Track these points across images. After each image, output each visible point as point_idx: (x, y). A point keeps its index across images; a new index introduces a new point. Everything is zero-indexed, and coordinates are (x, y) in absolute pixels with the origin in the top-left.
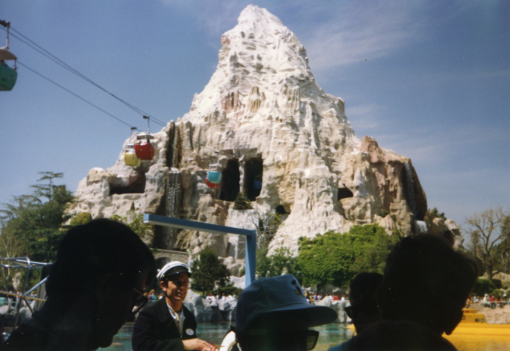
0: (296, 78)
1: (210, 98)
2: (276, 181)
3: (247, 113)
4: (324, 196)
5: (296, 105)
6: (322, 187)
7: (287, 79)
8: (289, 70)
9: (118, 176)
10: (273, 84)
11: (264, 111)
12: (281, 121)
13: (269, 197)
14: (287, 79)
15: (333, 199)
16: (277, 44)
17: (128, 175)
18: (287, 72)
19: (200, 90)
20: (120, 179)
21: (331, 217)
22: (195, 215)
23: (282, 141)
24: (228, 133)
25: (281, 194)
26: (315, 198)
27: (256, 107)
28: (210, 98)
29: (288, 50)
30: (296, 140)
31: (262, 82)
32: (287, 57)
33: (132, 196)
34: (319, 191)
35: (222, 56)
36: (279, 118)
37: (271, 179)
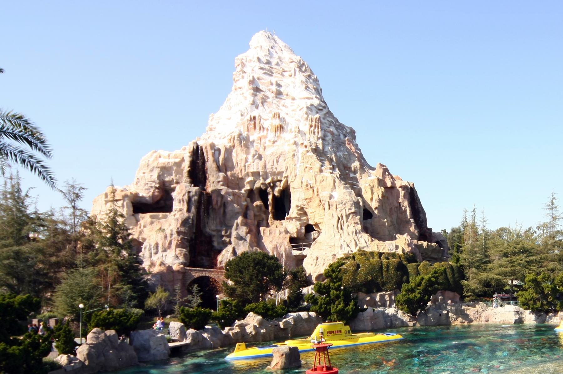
0: (315, 107)
1: (229, 119)
2: (305, 202)
3: (271, 135)
4: (352, 217)
5: (318, 133)
6: (350, 209)
7: (307, 108)
8: (308, 98)
9: (141, 195)
10: (293, 110)
11: (288, 136)
12: (306, 147)
13: (298, 216)
14: (307, 108)
15: (360, 219)
16: (293, 72)
17: (151, 194)
18: (307, 100)
19: (216, 110)
20: (143, 197)
21: (360, 235)
22: (228, 234)
23: (308, 166)
24: (254, 156)
25: (311, 214)
26: (345, 219)
27: (279, 132)
28: (229, 119)
29: (304, 79)
30: (322, 166)
31: (281, 107)
32: (304, 86)
33: (159, 215)
34: (348, 213)
35: (237, 79)
36: (304, 144)
37: (300, 201)
